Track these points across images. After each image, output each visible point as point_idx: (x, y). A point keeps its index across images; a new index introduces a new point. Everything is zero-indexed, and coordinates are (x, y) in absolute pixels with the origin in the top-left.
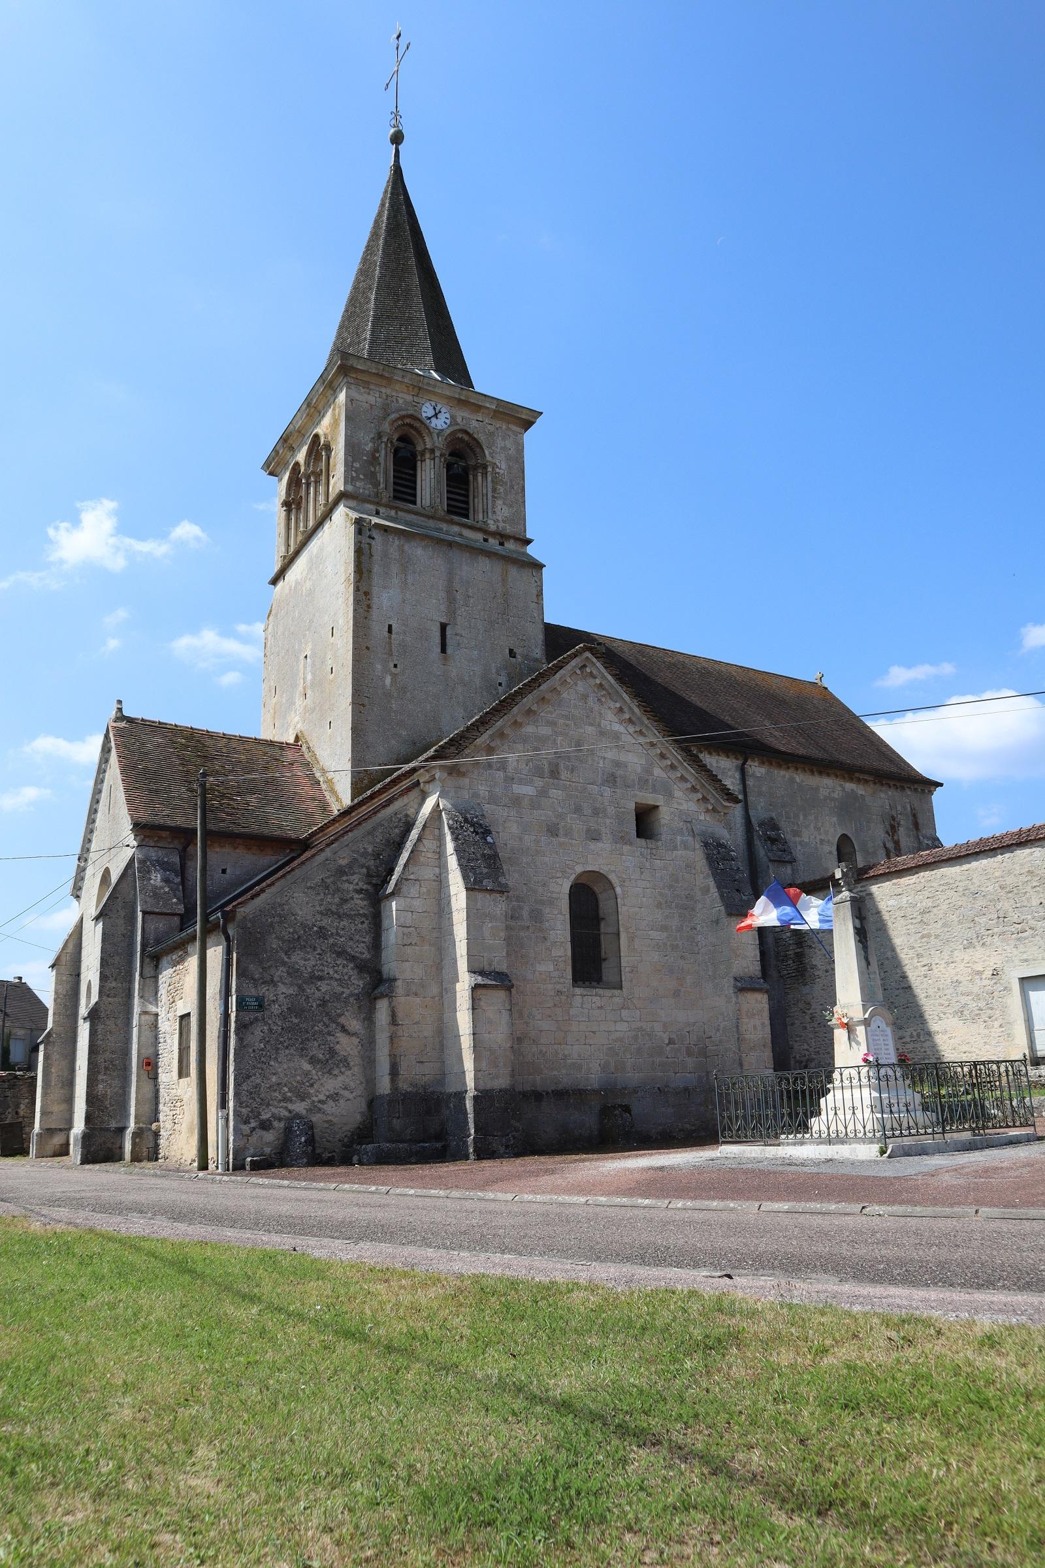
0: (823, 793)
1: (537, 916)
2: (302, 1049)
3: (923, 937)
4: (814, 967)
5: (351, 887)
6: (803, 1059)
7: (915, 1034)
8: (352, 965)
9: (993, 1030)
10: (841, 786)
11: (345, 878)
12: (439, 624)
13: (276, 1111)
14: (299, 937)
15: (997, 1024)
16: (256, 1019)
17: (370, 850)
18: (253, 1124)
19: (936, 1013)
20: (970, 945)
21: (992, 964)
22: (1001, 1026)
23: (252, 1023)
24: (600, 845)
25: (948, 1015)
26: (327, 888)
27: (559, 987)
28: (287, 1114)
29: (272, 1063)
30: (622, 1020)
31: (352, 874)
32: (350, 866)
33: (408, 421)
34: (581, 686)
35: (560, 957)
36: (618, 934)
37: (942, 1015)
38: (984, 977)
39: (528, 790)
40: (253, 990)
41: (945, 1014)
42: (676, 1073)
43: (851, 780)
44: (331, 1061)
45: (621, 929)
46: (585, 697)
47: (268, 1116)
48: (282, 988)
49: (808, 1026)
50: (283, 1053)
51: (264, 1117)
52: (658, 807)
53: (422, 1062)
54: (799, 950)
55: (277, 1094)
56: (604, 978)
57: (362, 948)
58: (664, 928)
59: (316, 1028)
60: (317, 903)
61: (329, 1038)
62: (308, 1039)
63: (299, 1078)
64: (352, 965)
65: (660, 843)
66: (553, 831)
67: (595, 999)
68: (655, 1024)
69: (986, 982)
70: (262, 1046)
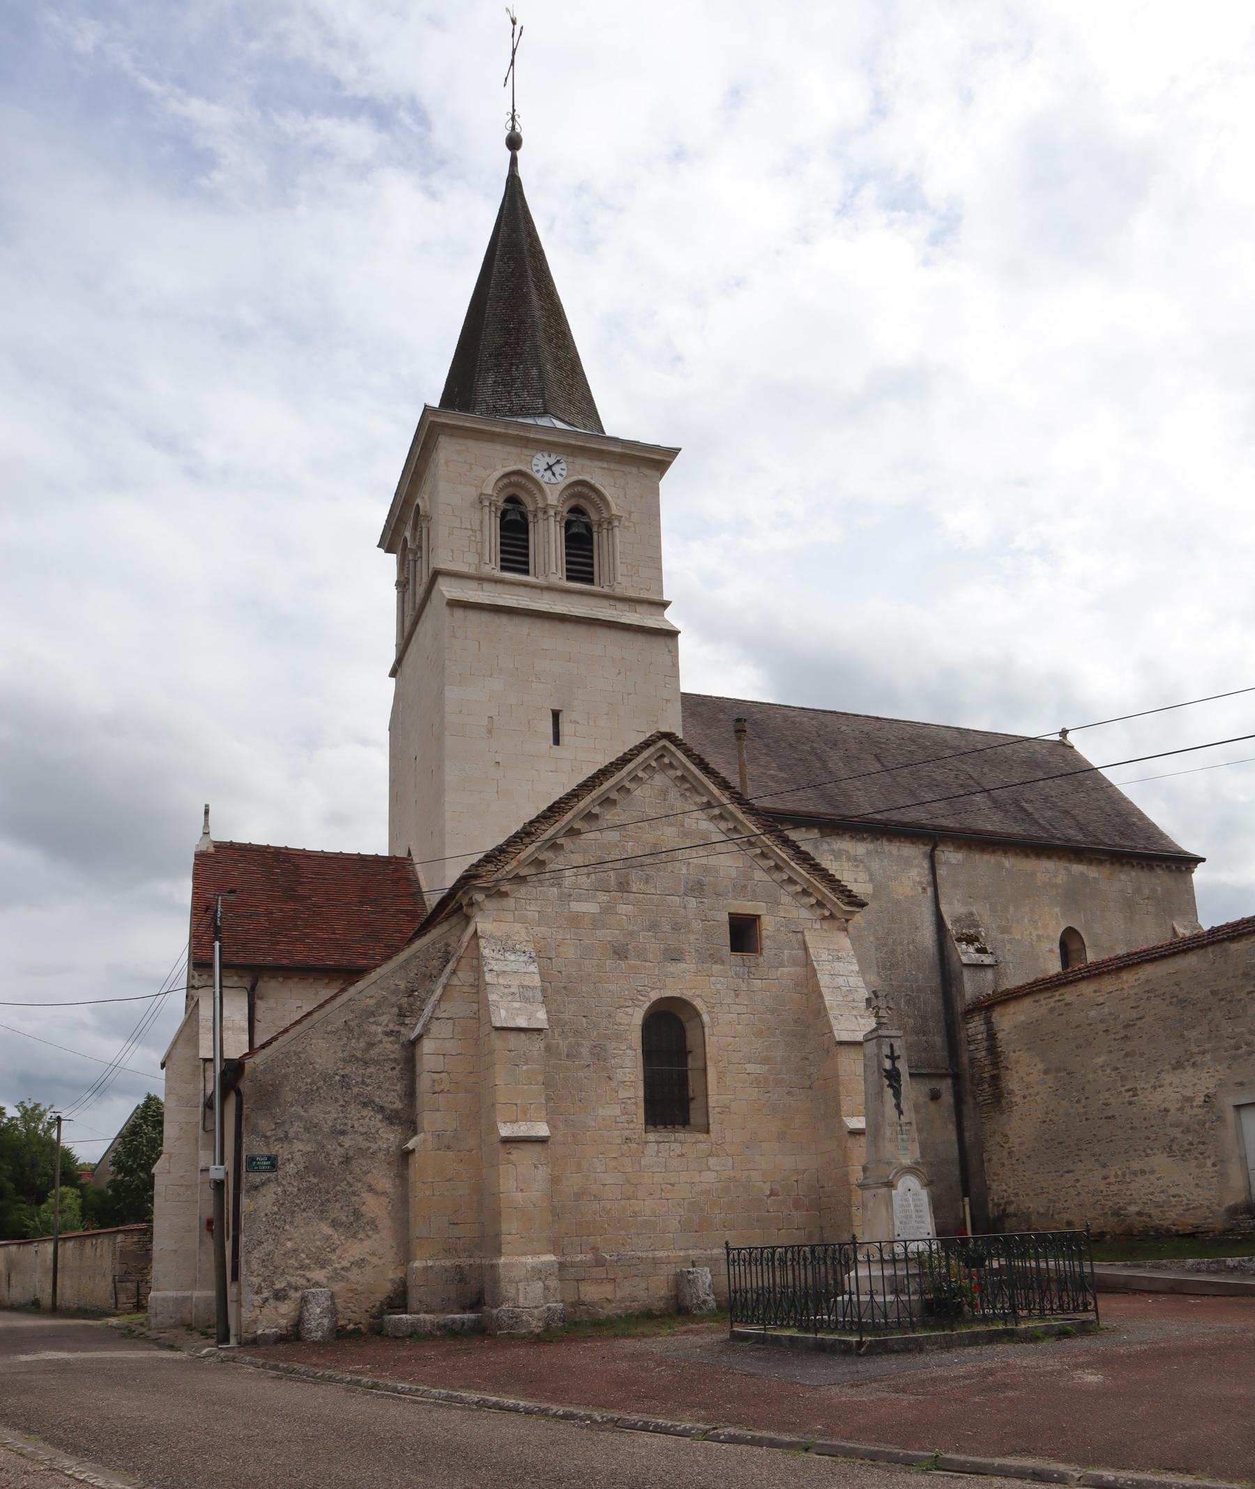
0: (1041, 878)
1: (599, 1053)
2: (322, 1212)
3: (1126, 1055)
4: (1011, 1092)
5: (380, 1029)
6: (1002, 1201)
7: (1119, 1173)
8: (380, 1117)
9: (1206, 1169)
10: (1066, 869)
11: (371, 1020)
12: (550, 712)
13: (292, 1280)
14: (318, 1088)
15: (1209, 1162)
16: (269, 1180)
17: (402, 987)
18: (266, 1295)
19: (1141, 1148)
20: (1178, 1066)
21: (1203, 1088)
22: (1214, 1165)
23: (263, 1184)
24: (683, 966)
25: (1155, 1151)
26: (351, 1031)
27: (627, 1133)
28: (304, 1282)
29: (287, 1227)
30: (709, 1169)
31: (381, 1015)
32: (379, 1005)
33: (514, 479)
34: (659, 780)
35: (630, 1098)
36: (705, 1070)
37: (1149, 1151)
38: (1195, 1104)
39: (590, 908)
40: (264, 1148)
41: (1152, 1149)
42: (779, 1230)
43: (1080, 861)
44: (355, 1224)
45: (709, 1063)
46: (664, 793)
47: (283, 1285)
48: (298, 1145)
49: (1006, 1163)
50: (299, 1217)
51: (278, 1286)
52: (759, 916)
53: (457, 1224)
54: (995, 1072)
55: (292, 1261)
56: (692, 1121)
57: (392, 1097)
58: (765, 1061)
59: (338, 1188)
60: (338, 1049)
61: (354, 1199)
62: (328, 1200)
63: (318, 1243)
64: (380, 1117)
65: (761, 959)
66: (620, 953)
67: (673, 1146)
68: (753, 1173)
69: (1197, 1111)
70: (275, 1209)
